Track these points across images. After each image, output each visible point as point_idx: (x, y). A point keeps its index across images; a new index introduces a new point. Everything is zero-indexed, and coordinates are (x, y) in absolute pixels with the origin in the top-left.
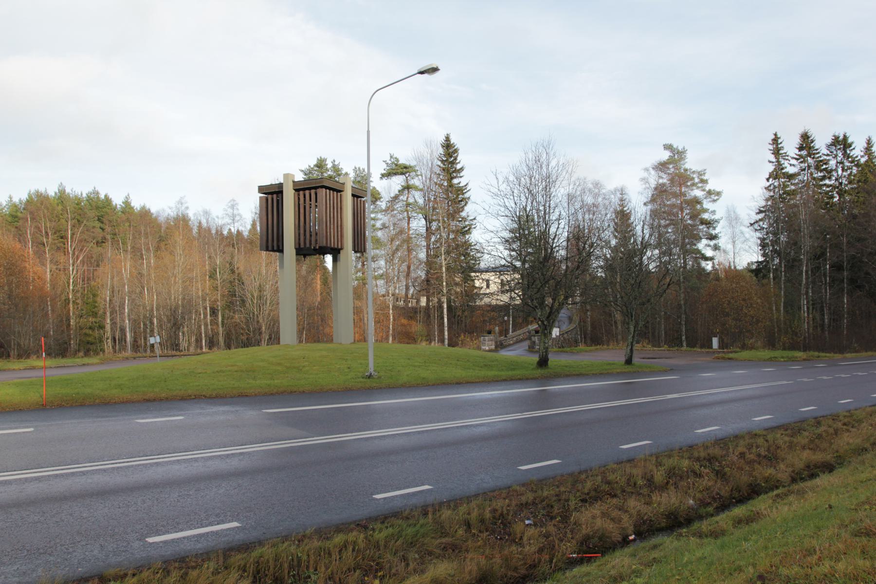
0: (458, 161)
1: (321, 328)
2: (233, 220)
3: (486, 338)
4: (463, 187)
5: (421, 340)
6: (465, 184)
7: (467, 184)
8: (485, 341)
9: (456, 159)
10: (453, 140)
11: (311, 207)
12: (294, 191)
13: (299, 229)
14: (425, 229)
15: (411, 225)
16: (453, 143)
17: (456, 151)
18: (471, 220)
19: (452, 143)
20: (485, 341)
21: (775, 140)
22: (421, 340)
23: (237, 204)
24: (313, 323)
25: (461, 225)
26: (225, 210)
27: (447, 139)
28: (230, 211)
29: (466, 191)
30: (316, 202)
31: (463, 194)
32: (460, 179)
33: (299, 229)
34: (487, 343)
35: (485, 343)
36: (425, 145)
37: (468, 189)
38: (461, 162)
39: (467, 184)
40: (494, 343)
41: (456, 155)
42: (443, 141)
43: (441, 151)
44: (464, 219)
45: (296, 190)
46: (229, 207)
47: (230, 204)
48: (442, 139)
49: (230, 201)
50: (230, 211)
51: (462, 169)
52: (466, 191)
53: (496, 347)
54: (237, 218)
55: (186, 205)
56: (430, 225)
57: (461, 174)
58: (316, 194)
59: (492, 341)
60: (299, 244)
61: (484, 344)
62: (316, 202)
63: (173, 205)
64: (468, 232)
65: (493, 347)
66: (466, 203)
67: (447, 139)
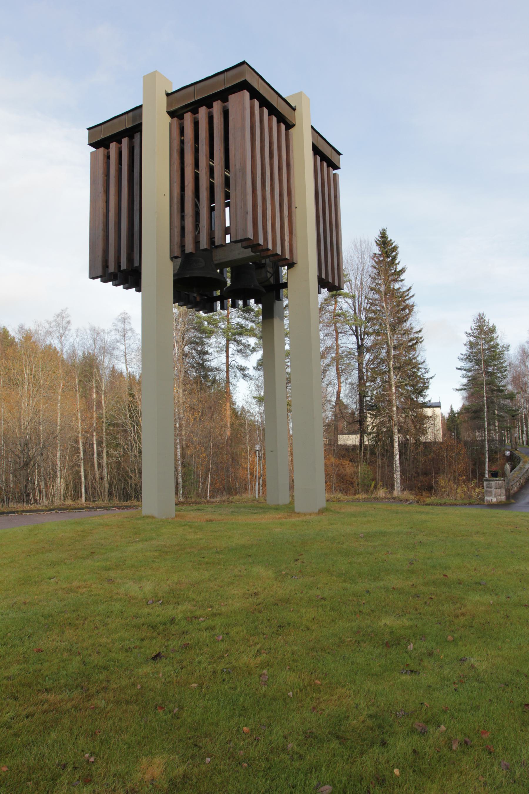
0: (397, 262)
1: (232, 470)
2: (124, 336)
3: (493, 483)
4: (404, 292)
5: (375, 487)
6: (408, 288)
7: (410, 288)
8: (491, 488)
9: (395, 258)
10: (390, 236)
11: (212, 209)
12: (168, 119)
13: (183, 218)
14: (356, 347)
15: (339, 342)
16: (391, 240)
17: (395, 248)
18: (417, 333)
19: (389, 239)
20: (491, 488)
21: (457, 369)
22: (375, 487)
23: (128, 317)
24: (221, 463)
25: (405, 338)
26: (114, 325)
27: (383, 235)
28: (120, 326)
29: (407, 297)
30: (227, 166)
31: (404, 301)
32: (400, 283)
33: (183, 218)
34: (493, 491)
35: (491, 492)
36: (353, 247)
37: (410, 295)
38: (401, 263)
39: (410, 288)
40: (503, 491)
41: (394, 253)
42: (378, 238)
43: (376, 250)
44: (407, 332)
45: (172, 114)
46: (119, 321)
47: (120, 318)
48: (376, 235)
49: (121, 314)
50: (120, 326)
51: (403, 271)
52: (407, 297)
53: (508, 497)
54: (129, 334)
55: (68, 319)
56: (361, 342)
57: (402, 277)
58: (226, 113)
59: (500, 488)
60: (183, 247)
61: (490, 494)
62: (227, 166)
63: (51, 319)
64: (413, 347)
65: (503, 498)
66: (411, 311)
67: (383, 235)
